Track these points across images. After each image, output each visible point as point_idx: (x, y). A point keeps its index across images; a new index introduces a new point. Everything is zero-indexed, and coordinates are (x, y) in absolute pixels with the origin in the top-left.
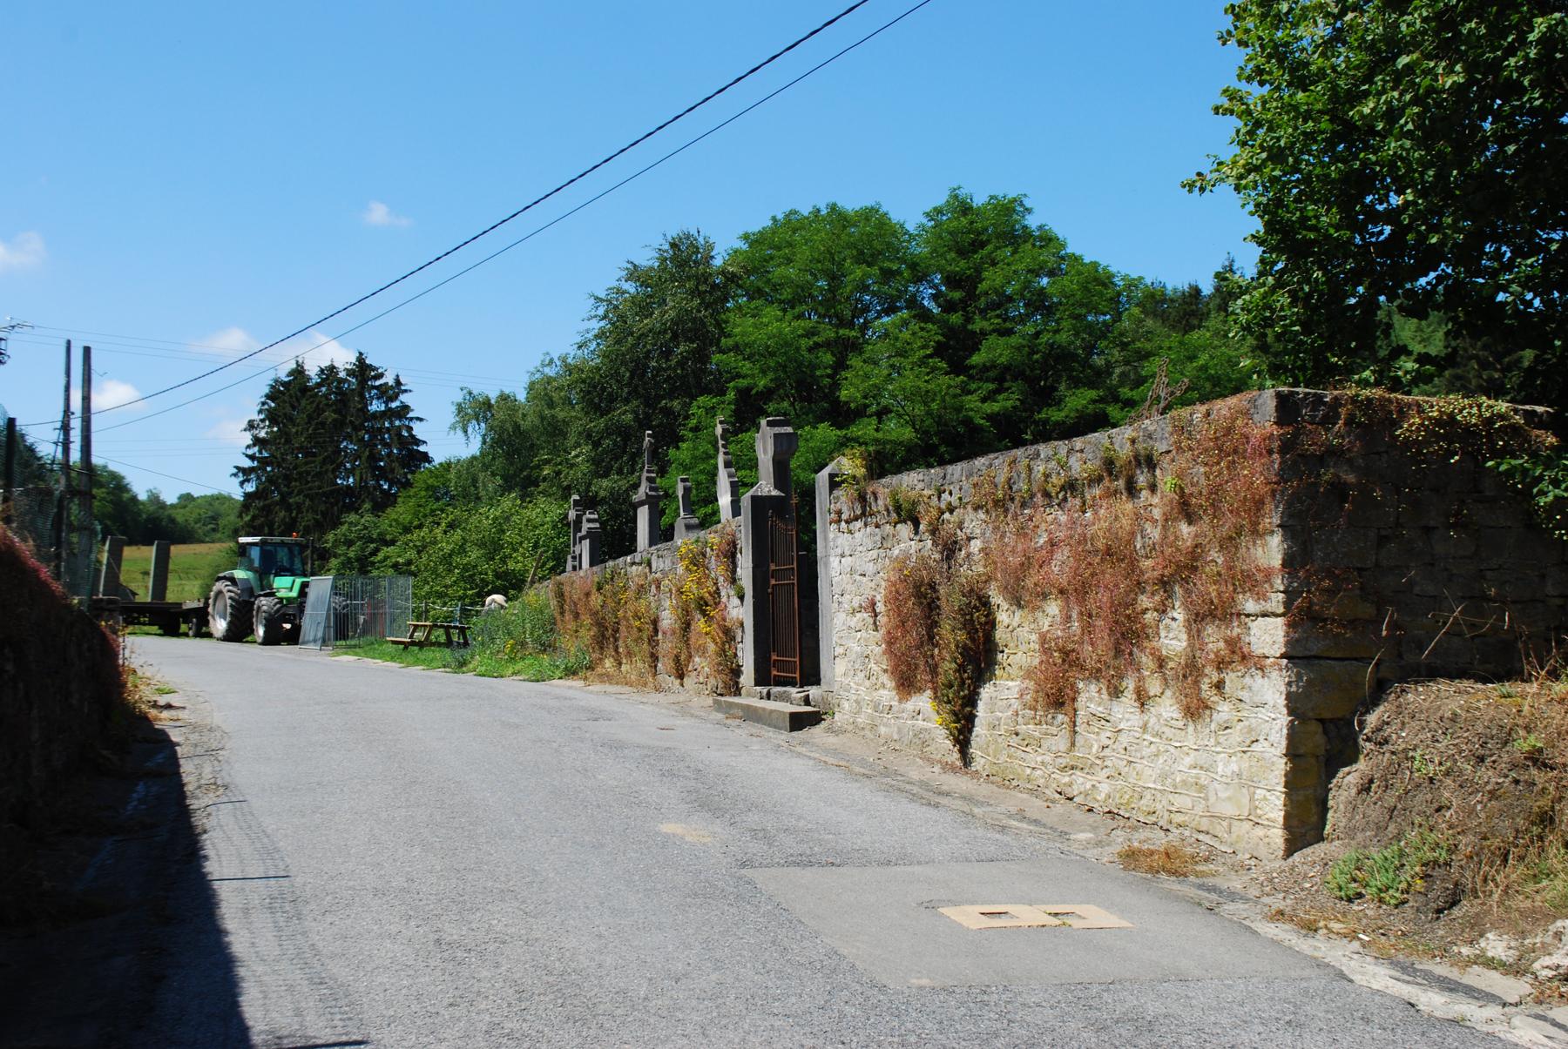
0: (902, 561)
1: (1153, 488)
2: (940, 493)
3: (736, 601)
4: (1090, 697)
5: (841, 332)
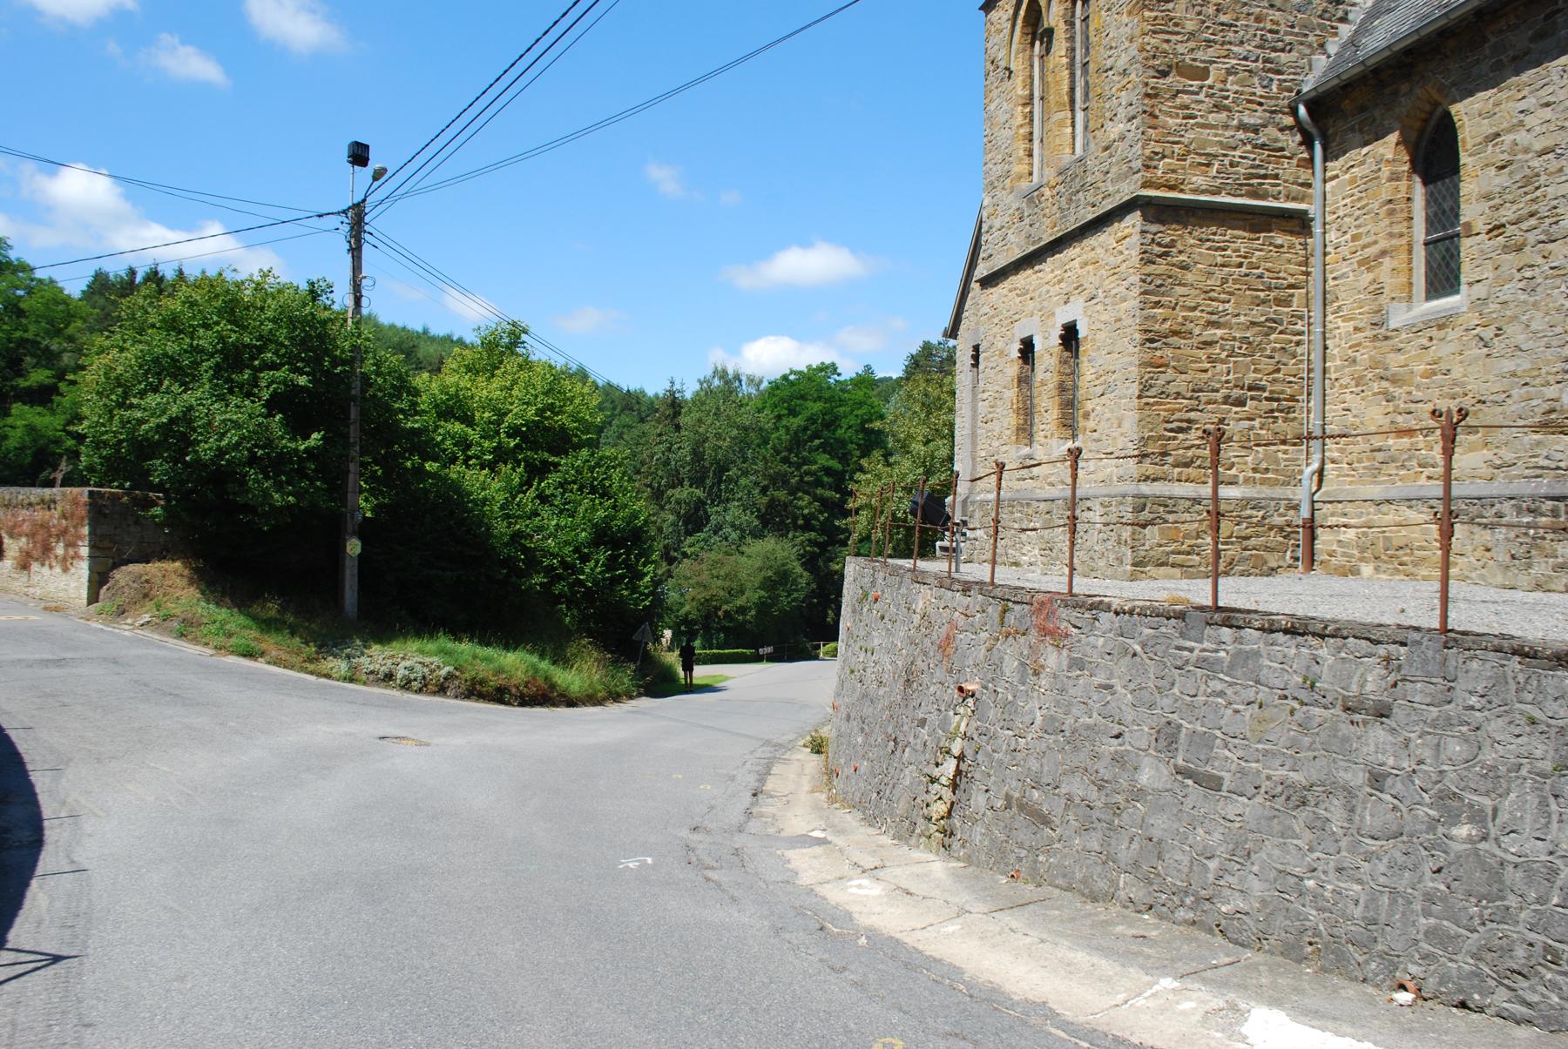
4: (35, 566)
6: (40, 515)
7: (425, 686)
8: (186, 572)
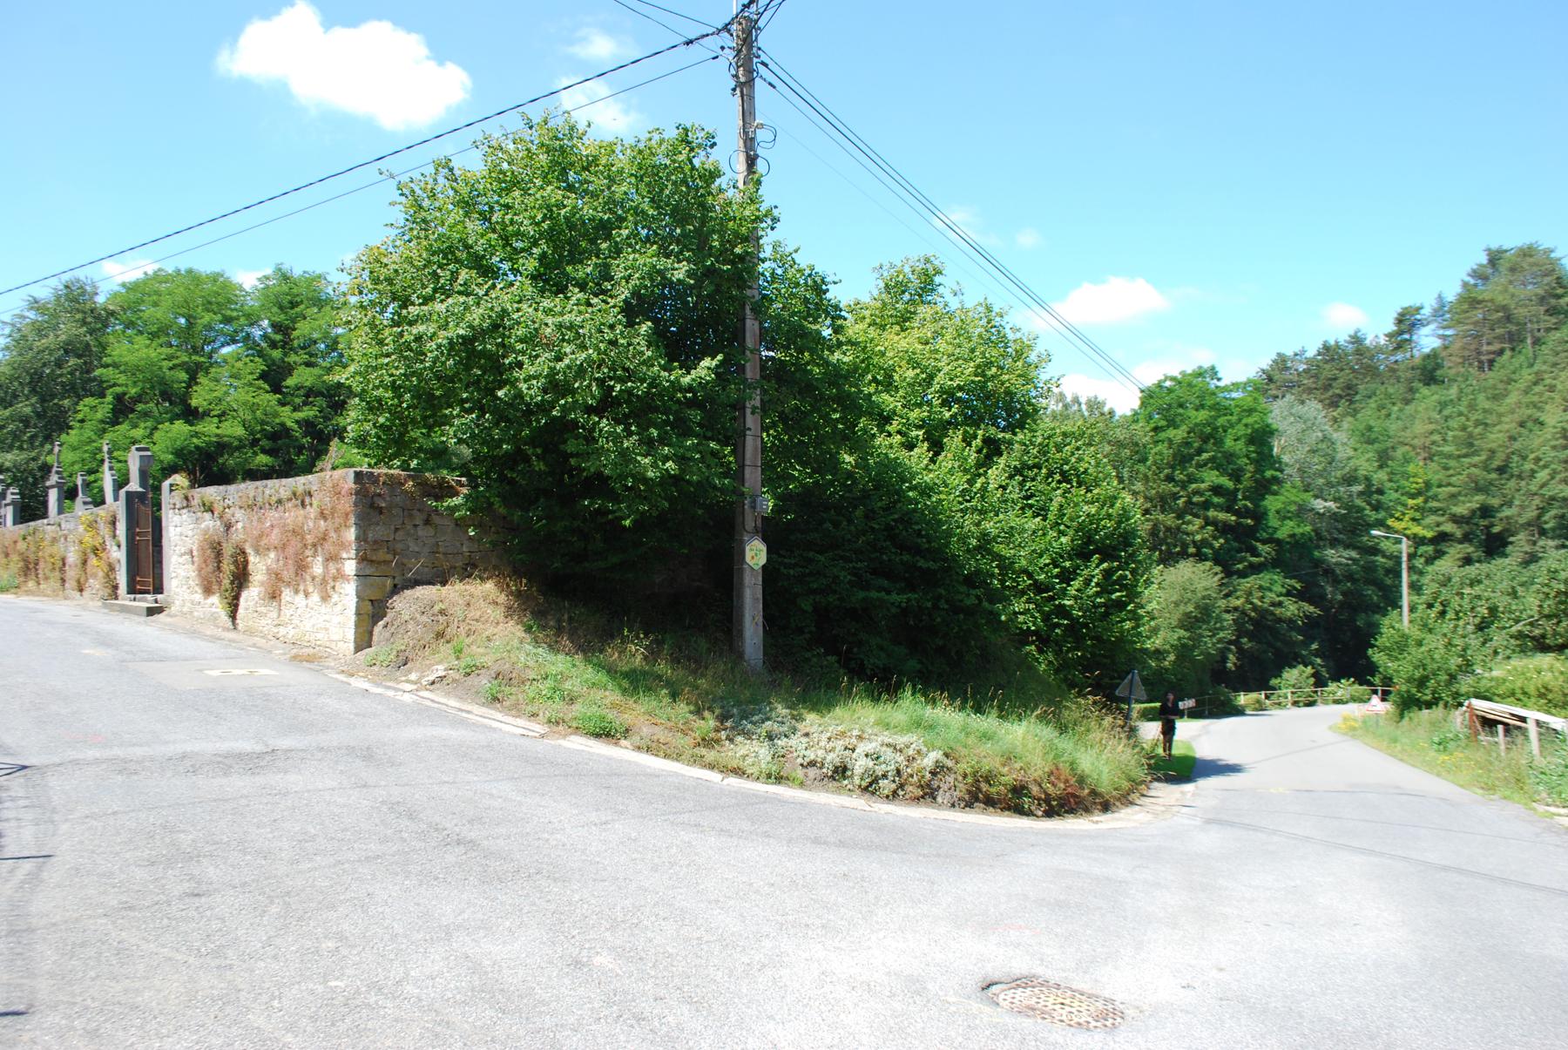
0: (206, 531)
1: (311, 504)
2: (224, 499)
3: (115, 548)
4: (287, 594)
5: (193, 357)
6: (292, 515)
7: (902, 786)
8: (502, 598)
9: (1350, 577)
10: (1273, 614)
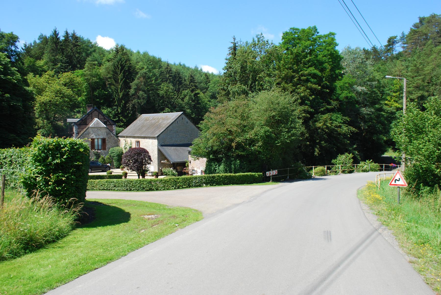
9: (371, 119)
10: (337, 131)
